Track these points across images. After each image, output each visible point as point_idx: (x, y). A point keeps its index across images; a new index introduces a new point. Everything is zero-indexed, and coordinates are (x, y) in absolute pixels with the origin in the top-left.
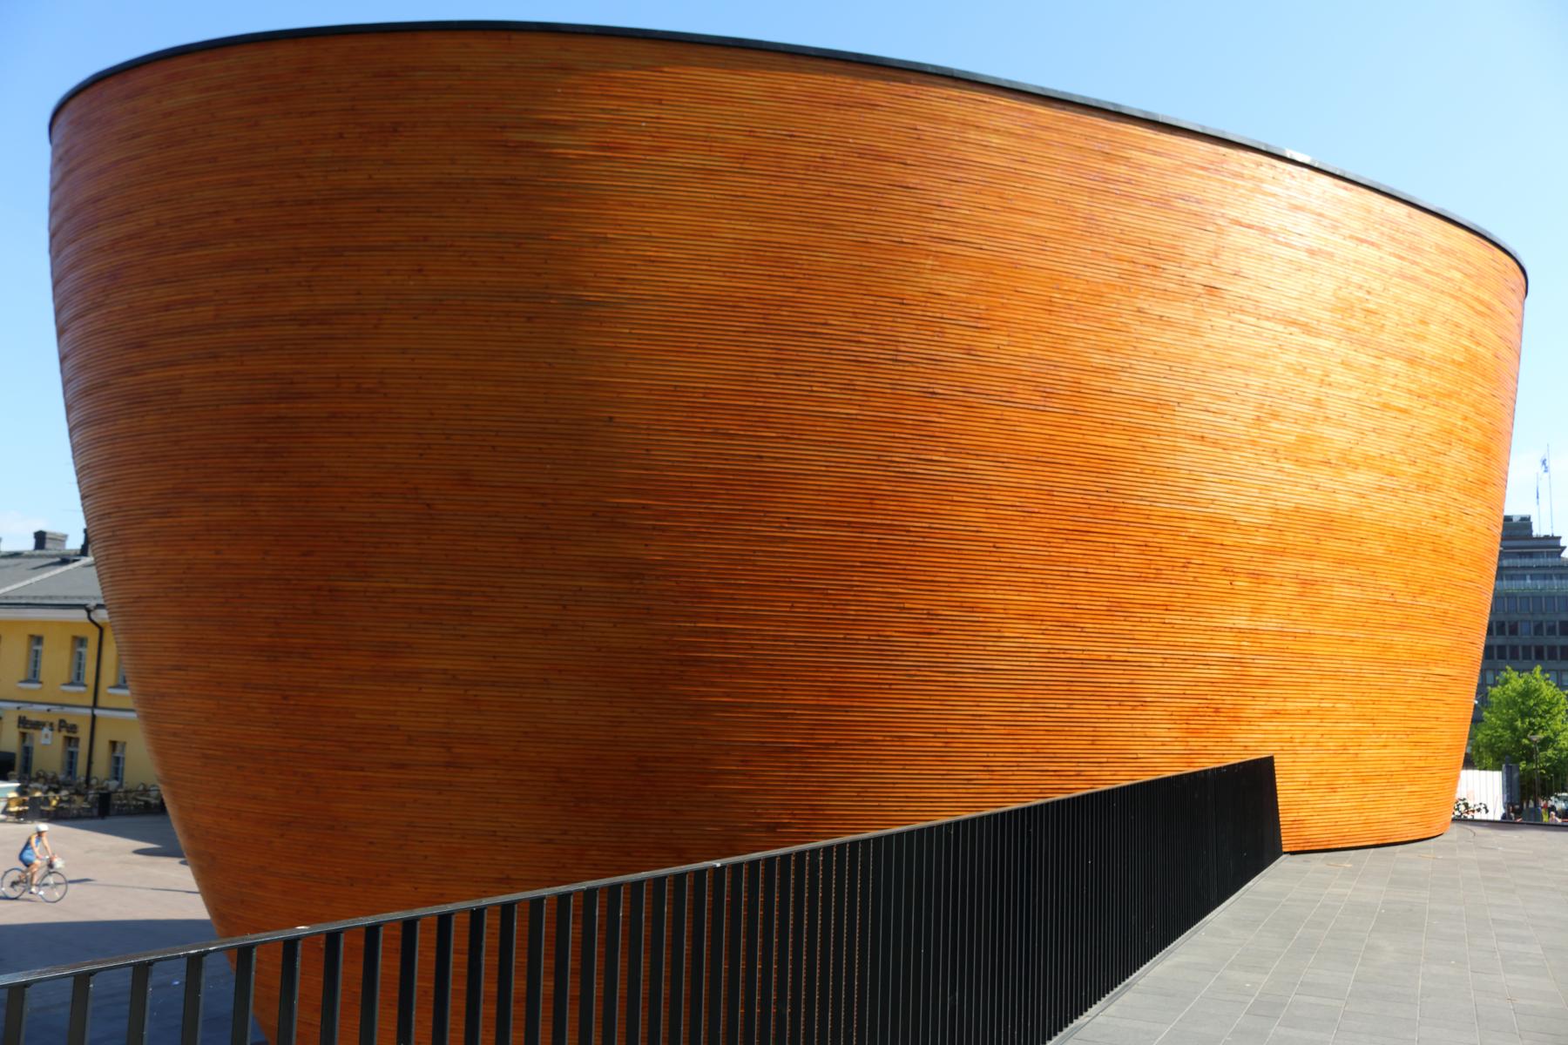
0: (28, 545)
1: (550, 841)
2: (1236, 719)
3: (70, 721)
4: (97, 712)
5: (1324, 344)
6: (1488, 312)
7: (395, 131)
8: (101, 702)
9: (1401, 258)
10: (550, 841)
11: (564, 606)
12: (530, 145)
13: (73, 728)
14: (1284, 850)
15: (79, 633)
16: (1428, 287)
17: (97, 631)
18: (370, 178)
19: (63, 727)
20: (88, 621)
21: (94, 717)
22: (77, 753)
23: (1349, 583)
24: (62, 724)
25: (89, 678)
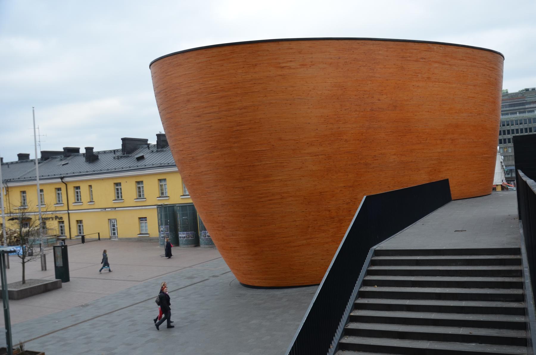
0: (16, 159)
1: (303, 212)
2: (439, 172)
3: (59, 216)
4: (69, 212)
5: (454, 86)
6: (493, 69)
7: (256, 66)
8: (70, 208)
9: (471, 62)
10: (303, 212)
11: (303, 163)
12: (285, 67)
13: (61, 218)
14: (452, 199)
15: (58, 187)
16: (478, 67)
17: (65, 185)
18: (252, 76)
19: (57, 218)
20: (62, 182)
21: (69, 213)
22: (64, 226)
23: (463, 139)
24: (57, 217)
25: (65, 201)
